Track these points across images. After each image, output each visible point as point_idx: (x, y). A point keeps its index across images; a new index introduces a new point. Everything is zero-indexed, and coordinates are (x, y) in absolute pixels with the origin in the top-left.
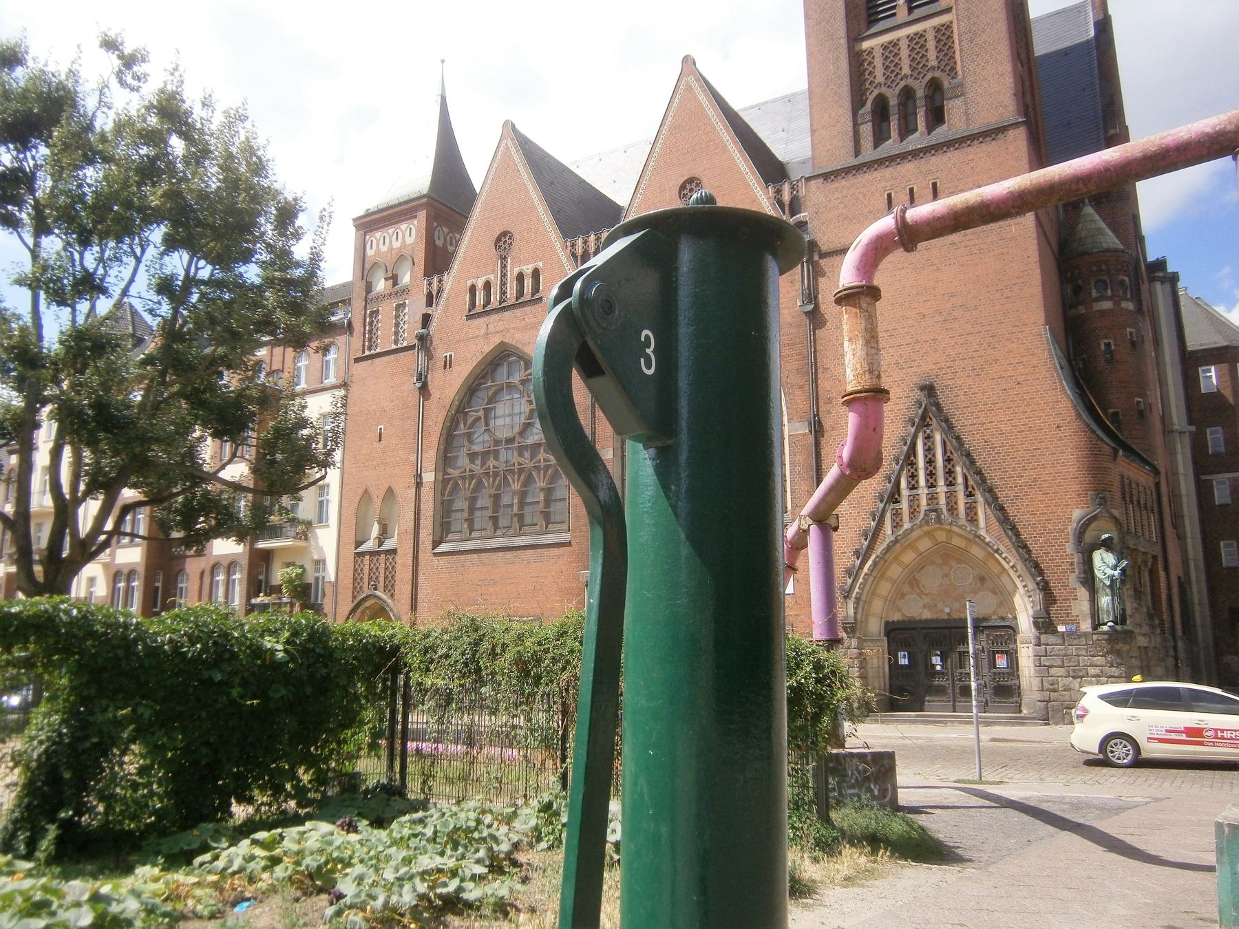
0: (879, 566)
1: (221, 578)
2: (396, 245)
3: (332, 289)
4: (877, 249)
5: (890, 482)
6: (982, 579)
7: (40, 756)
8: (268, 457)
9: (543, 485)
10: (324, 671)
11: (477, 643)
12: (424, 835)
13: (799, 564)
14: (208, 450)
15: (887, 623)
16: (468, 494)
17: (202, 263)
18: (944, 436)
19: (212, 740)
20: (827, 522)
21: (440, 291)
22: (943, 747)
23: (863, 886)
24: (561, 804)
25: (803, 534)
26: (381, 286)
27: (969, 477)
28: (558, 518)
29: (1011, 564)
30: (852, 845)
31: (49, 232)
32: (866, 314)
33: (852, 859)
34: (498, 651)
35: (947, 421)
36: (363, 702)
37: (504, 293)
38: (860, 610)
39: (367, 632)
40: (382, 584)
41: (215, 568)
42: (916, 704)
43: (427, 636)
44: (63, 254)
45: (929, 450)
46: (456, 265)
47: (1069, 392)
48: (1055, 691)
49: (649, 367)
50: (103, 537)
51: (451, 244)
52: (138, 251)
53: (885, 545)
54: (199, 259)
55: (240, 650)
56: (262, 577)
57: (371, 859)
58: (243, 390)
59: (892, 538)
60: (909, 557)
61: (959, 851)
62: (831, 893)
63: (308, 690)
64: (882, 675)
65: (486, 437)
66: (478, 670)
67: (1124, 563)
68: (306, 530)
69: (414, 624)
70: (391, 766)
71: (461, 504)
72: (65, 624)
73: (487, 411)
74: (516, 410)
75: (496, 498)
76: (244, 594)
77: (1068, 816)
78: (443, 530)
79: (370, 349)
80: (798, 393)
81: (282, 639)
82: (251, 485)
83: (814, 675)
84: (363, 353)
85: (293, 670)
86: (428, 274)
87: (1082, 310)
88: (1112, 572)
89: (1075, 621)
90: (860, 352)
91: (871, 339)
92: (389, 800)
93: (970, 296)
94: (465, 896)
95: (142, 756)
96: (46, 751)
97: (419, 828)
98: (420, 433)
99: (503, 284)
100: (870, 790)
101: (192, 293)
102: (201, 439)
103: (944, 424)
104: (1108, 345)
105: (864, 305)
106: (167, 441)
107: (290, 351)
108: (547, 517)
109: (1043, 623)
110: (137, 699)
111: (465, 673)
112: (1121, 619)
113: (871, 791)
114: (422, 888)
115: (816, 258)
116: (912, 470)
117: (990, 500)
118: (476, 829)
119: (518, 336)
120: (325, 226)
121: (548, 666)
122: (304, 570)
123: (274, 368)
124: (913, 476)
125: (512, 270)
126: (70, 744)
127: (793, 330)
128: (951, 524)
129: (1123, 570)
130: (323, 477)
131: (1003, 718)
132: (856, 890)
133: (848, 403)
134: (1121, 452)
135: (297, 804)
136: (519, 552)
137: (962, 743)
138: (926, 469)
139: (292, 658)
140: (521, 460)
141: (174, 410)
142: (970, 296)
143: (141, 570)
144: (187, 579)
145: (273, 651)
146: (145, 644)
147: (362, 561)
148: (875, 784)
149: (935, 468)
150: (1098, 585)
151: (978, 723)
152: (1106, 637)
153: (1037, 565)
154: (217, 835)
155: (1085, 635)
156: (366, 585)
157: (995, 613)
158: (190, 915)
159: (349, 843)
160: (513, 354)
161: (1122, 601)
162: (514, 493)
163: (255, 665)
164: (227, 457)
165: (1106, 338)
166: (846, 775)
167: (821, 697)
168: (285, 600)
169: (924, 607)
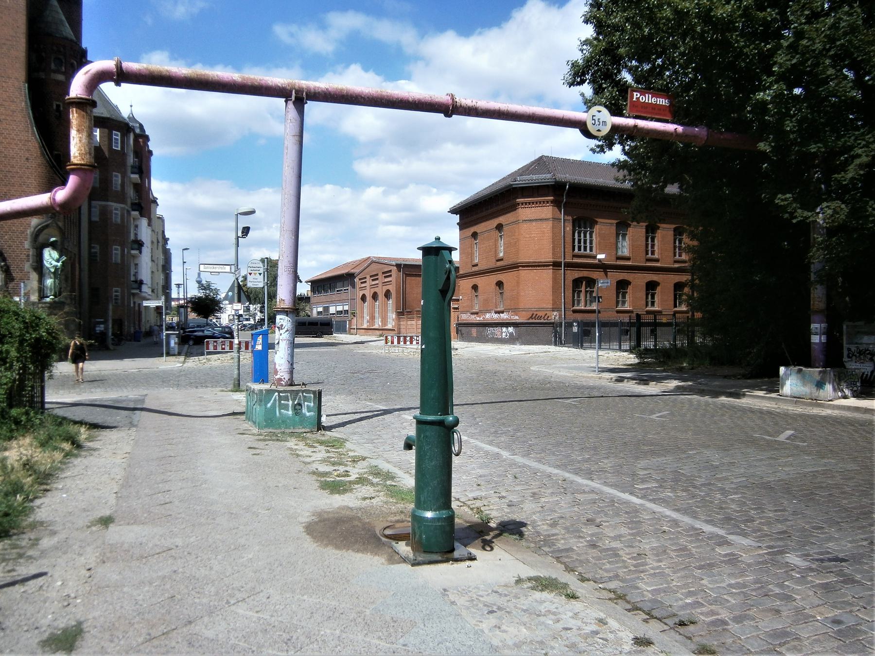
67: (64, 258)
88: (56, 264)
104: (58, 106)
150: (45, 270)
165: (58, 101)
167: (51, 344)
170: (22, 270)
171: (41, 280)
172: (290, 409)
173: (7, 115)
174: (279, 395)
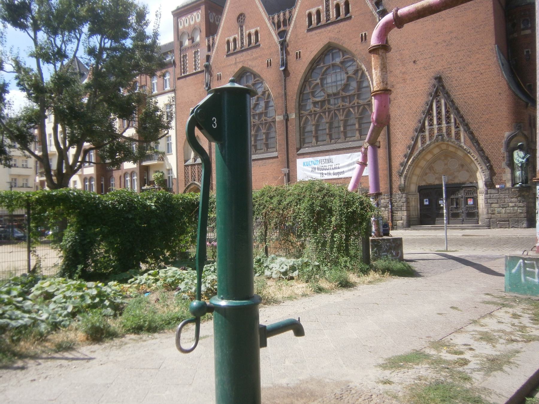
0: (415, 162)
1: (128, 178)
2: (192, 23)
3: (165, 46)
4: (386, 28)
5: (420, 123)
6: (462, 166)
7: (69, 246)
9: (264, 131)
10: (171, 213)
14: (117, 124)
15: (419, 187)
17: (106, 40)
18: (445, 101)
19: (130, 240)
20: (375, 144)
21: (213, 43)
22: (438, 239)
23: (375, 284)
26: (187, 43)
27: (457, 119)
28: (272, 146)
29: (475, 158)
31: (39, 29)
32: (381, 57)
33: (373, 275)
35: (447, 93)
36: (188, 225)
37: (242, 43)
38: (407, 181)
39: (187, 197)
40: (197, 178)
41: (125, 174)
44: (48, 41)
45: (439, 107)
46: (220, 31)
47: (505, 77)
48: (494, 214)
49: (215, 126)
50: (78, 164)
51: (217, 21)
52: (78, 36)
53: (417, 152)
54: (105, 39)
55: (138, 206)
56: (146, 178)
59: (421, 149)
60: (429, 157)
61: (421, 274)
64: (416, 209)
67: (528, 156)
68: (162, 156)
72: (72, 198)
76: (139, 185)
79: (184, 73)
81: (153, 201)
82: (137, 138)
84: (181, 75)
86: (208, 35)
87: (515, 35)
91: (384, 68)
93: (459, 32)
95: (106, 246)
96: (71, 245)
99: (242, 39)
100: (392, 253)
101: (103, 54)
102: (114, 119)
103: (446, 95)
105: (380, 53)
106: (100, 122)
108: (267, 146)
110: (102, 225)
113: (392, 253)
116: (431, 117)
119: (250, 63)
120: (159, 19)
121: (257, 207)
122: (163, 174)
123: (143, 84)
124: (431, 120)
125: (246, 32)
126: (79, 242)
128: (448, 141)
129: (527, 160)
134: (530, 104)
135: (164, 263)
138: (437, 116)
141: (101, 108)
142: (459, 32)
143: (95, 177)
144: (114, 180)
145: (150, 206)
146: (102, 205)
147: (188, 169)
148: (394, 251)
150: (516, 166)
151: (447, 229)
152: (518, 189)
153: (487, 158)
155: (508, 189)
156: (190, 179)
157: (468, 180)
159: (183, 273)
160: (248, 72)
161: (526, 173)
164: (126, 127)
165: (527, 49)
166: (382, 248)
167: (362, 215)
168: (156, 187)
169: (436, 179)
170: (500, 167)
171: (513, 173)
172: (536, 277)
173: (486, 69)
174: (524, 263)
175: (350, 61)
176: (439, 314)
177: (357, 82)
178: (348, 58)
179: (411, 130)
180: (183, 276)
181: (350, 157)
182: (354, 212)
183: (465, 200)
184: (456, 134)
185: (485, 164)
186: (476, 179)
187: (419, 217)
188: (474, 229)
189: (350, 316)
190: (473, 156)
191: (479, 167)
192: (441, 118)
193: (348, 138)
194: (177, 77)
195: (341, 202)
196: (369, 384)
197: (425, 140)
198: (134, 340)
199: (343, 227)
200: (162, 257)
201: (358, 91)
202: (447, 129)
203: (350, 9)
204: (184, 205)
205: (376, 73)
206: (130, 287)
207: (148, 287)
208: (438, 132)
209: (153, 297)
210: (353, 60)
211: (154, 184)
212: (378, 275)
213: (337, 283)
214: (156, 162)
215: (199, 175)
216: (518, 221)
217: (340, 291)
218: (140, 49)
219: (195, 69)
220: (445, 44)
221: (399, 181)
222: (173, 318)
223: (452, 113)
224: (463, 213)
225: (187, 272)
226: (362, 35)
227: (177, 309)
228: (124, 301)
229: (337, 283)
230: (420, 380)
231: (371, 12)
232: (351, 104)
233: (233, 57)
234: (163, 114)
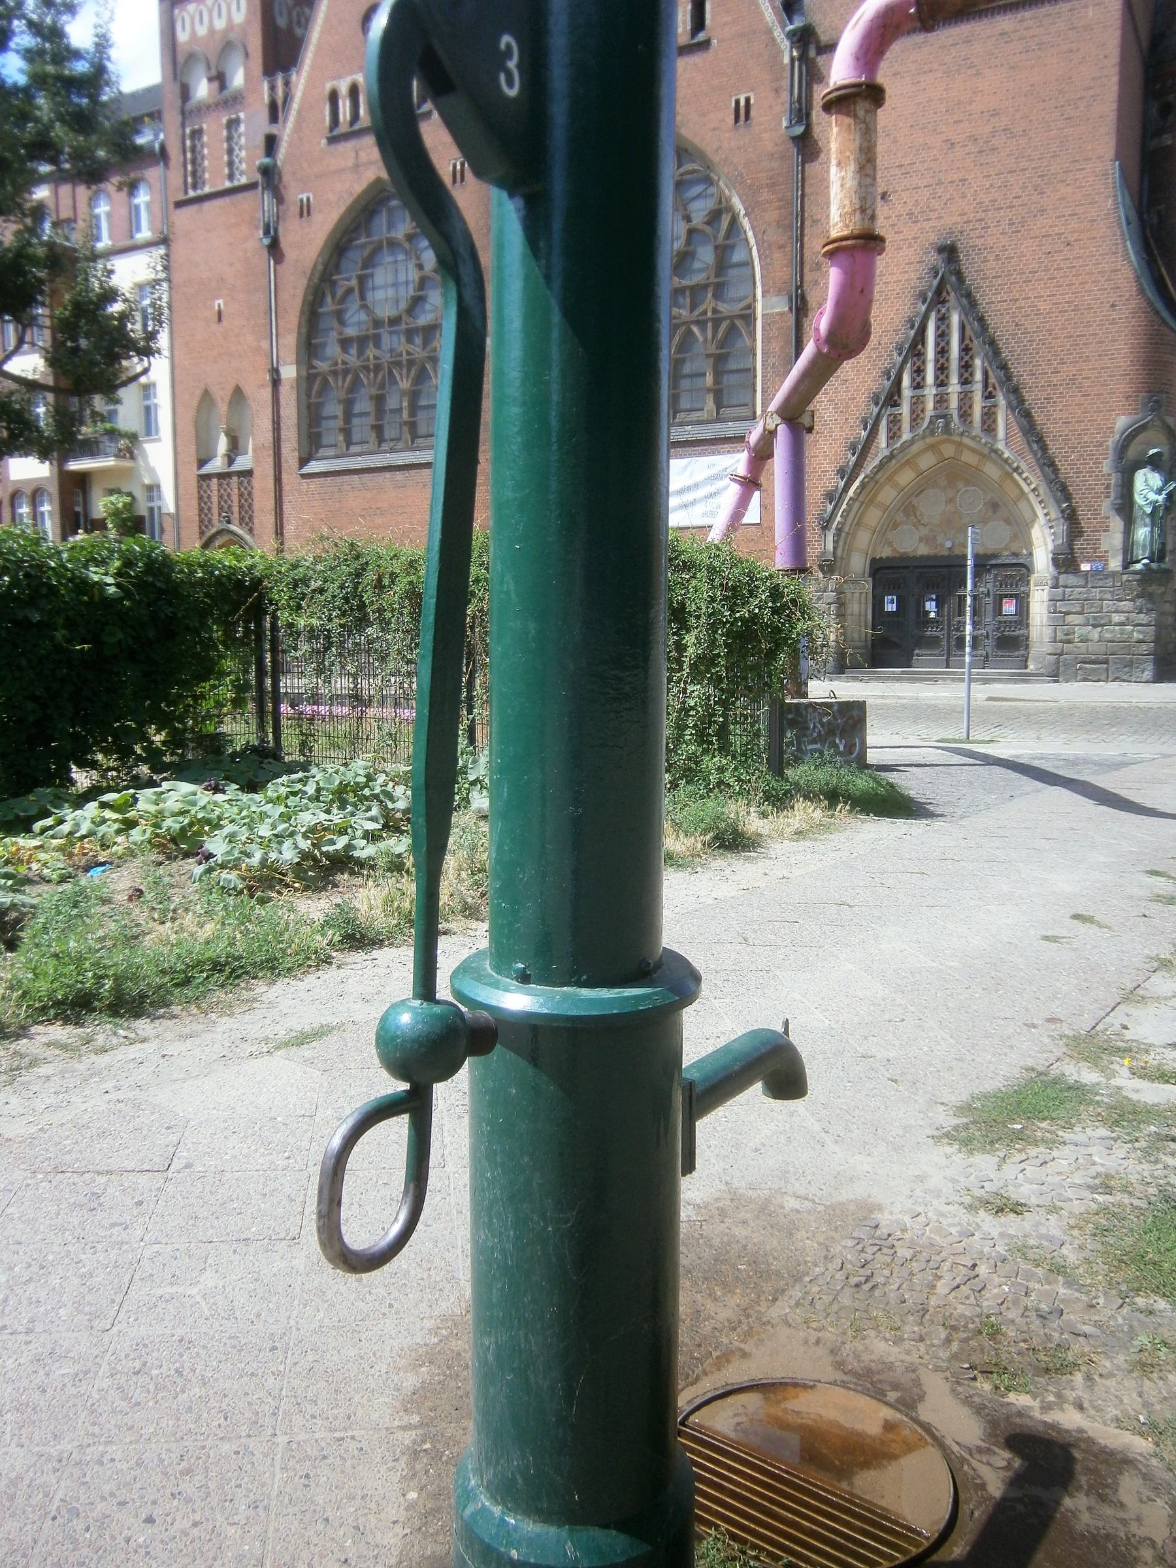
2: (220, 24)
3: (134, 96)
4: (885, 26)
5: (888, 379)
6: (995, 506)
8: (69, 344)
10: (169, 610)
11: (358, 574)
12: (305, 793)
13: (763, 480)
15: (873, 561)
16: (342, 395)
18: (963, 317)
20: (800, 420)
21: (287, 98)
22: (929, 706)
23: (816, 840)
24: (467, 761)
25: (769, 436)
26: (202, 90)
27: (990, 373)
29: (1033, 486)
30: (806, 797)
32: (863, 126)
33: (804, 813)
34: (386, 582)
35: (969, 295)
38: (841, 543)
39: (219, 562)
40: (236, 515)
42: (905, 661)
43: (295, 566)
46: (309, 57)
48: (1069, 642)
49: (510, 84)
53: (876, 462)
56: (78, 509)
57: (243, 818)
58: (23, 247)
59: (887, 453)
60: (906, 477)
62: (778, 846)
63: (152, 634)
65: (363, 316)
66: (362, 606)
68: (130, 446)
69: (280, 551)
70: (261, 726)
71: (334, 408)
73: (362, 280)
74: (402, 278)
75: (380, 400)
77: (1061, 773)
78: (311, 446)
79: (195, 187)
80: (777, 255)
81: (112, 570)
82: (50, 381)
83: (770, 604)
84: (186, 192)
85: (129, 609)
89: (1104, 558)
90: (851, 183)
91: (867, 162)
92: (261, 763)
94: (356, 854)
97: (299, 786)
98: (273, 311)
103: (964, 301)
105: (861, 113)
107: (82, 192)
109: (1064, 560)
111: (346, 611)
112: (1158, 556)
113: (837, 746)
114: (305, 845)
115: (812, 53)
117: (1015, 403)
118: (366, 785)
122: (134, 498)
124: (919, 371)
127: (775, 164)
128: (962, 434)
129: (1170, 496)
130: (145, 371)
131: (1003, 674)
132: (807, 843)
133: (830, 255)
136: (413, 472)
137: (953, 702)
138: (937, 361)
139: (127, 594)
140: (410, 348)
142: (1018, 116)
145: (102, 585)
147: (208, 486)
149: (948, 360)
150: (1137, 513)
151: (970, 680)
152: (1138, 577)
153: (1064, 489)
154: (58, 802)
155: (1114, 574)
156: (215, 517)
157: (1006, 548)
158: (37, 879)
159: (215, 803)
161: (1162, 534)
162: (403, 393)
163: (82, 603)
166: (807, 728)
167: (777, 630)
170: (1096, 514)
175: (698, 182)
176: (1046, 938)
177: (716, 248)
178: (693, 172)
179: (862, 398)
180: (218, 811)
181: (685, 468)
182: (754, 618)
183: (994, 603)
184: (986, 414)
185: (1058, 502)
186: (1029, 544)
187: (869, 643)
188: (1016, 682)
189: (778, 947)
190: (1025, 480)
191: (1040, 512)
192: (947, 368)
193: (683, 415)
194: (172, 200)
195: (713, 587)
196: (943, 1215)
197: (899, 429)
198: (64, 1047)
199: (717, 665)
200: (143, 748)
201: (717, 276)
202: (960, 400)
203: (708, 15)
204: (209, 585)
205: (843, 178)
206: (41, 847)
207: (102, 846)
208: (935, 408)
209: (121, 881)
210: (708, 181)
211: (106, 528)
212: (819, 811)
213: (708, 837)
214: (109, 462)
215: (241, 507)
216: (1130, 664)
217: (719, 863)
218: (54, 89)
219: (231, 177)
220: (972, 148)
221: (821, 545)
222: (199, 963)
223: (979, 353)
224: (987, 637)
225: (226, 797)
226: (737, 102)
227: (210, 928)
228: (19, 898)
229: (708, 837)
230: (1108, 1189)
231: (769, 31)
232: (696, 313)
233: (347, 147)
234: (132, 310)
